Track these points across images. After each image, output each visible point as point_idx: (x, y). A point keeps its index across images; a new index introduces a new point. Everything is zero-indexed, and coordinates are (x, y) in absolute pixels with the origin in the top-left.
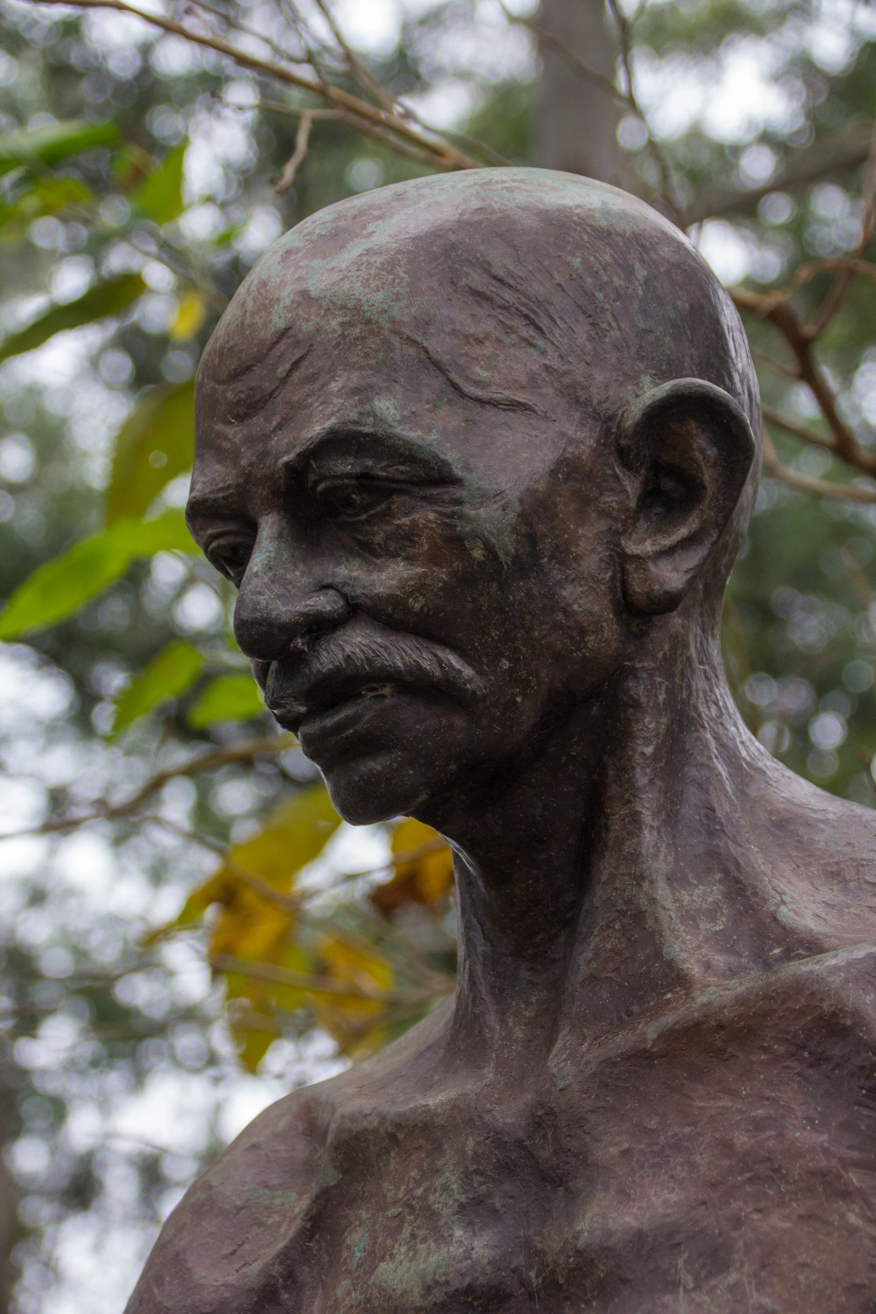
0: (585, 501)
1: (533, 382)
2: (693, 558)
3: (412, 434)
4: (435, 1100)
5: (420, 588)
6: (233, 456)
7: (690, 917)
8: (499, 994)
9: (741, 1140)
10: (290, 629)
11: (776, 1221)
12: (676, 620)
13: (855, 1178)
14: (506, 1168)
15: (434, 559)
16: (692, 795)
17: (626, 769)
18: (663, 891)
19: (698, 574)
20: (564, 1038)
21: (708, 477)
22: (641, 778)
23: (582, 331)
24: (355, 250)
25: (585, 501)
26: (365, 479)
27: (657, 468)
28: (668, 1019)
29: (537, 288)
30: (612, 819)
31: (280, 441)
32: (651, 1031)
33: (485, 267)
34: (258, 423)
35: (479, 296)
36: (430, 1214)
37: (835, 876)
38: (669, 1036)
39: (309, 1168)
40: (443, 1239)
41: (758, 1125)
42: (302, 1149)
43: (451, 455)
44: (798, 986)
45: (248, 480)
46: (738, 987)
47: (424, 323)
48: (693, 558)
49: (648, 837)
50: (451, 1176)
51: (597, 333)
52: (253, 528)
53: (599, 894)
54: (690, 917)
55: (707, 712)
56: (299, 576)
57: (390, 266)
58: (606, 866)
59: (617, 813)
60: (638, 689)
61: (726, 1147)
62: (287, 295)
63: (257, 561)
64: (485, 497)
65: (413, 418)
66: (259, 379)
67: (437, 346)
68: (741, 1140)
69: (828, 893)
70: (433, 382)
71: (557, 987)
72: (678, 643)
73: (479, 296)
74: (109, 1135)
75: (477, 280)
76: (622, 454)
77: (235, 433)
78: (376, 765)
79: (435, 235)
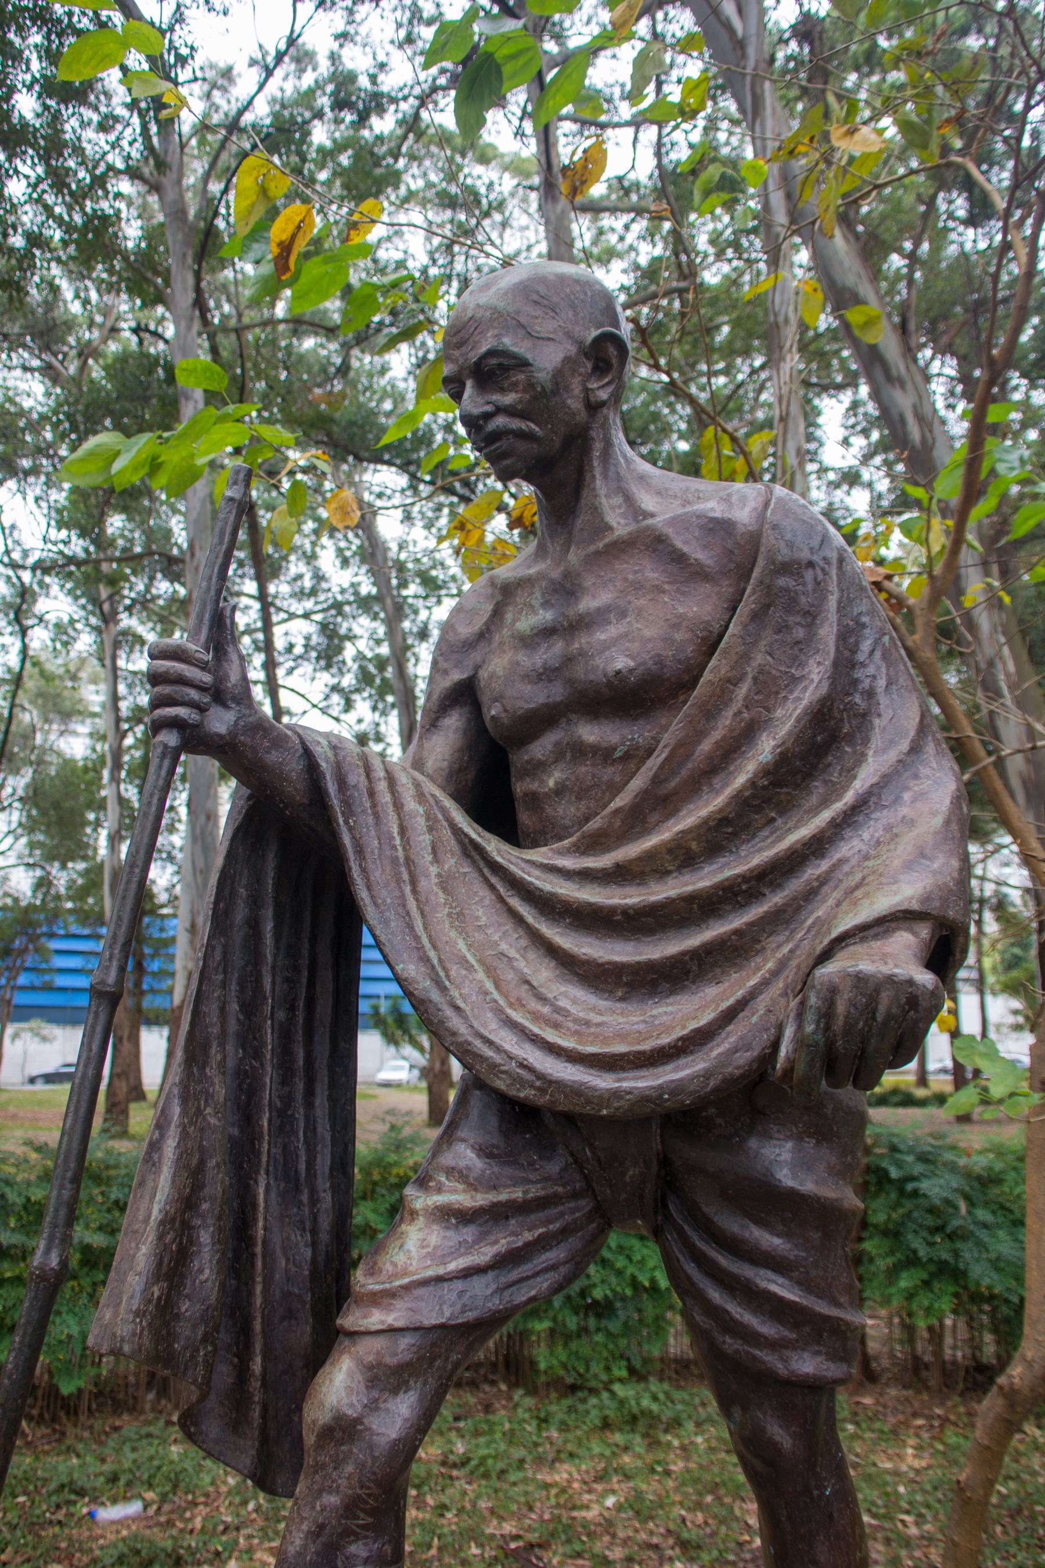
0: (574, 371)
1: (555, 332)
2: (610, 389)
3: (515, 349)
4: (532, 571)
5: (520, 401)
6: (456, 361)
7: (613, 508)
8: (551, 537)
9: (631, 577)
10: (478, 417)
11: (642, 601)
12: (605, 410)
13: (666, 587)
14: (555, 591)
15: (524, 391)
16: (612, 469)
17: (590, 460)
18: (603, 500)
19: (612, 395)
20: (573, 549)
21: (615, 361)
22: (596, 463)
23: (571, 314)
24: (494, 289)
25: (574, 371)
26: (500, 365)
27: (598, 359)
28: (606, 541)
29: (555, 299)
30: (535, 800)
31: (471, 354)
32: (601, 545)
33: (537, 293)
34: (464, 349)
35: (536, 303)
36: (532, 607)
37: (659, 493)
38: (607, 546)
39: (492, 596)
40: (535, 613)
41: (636, 572)
42: (490, 591)
43: (529, 356)
44: (648, 527)
45: (461, 369)
46: (629, 529)
47: (518, 312)
48: (610, 389)
49: (598, 483)
50: (538, 594)
51: (576, 314)
52: (463, 385)
53: (583, 502)
54: (613, 508)
55: (616, 441)
56: (480, 400)
57: (506, 294)
58: (585, 493)
59: (588, 476)
60: (593, 434)
61: (626, 579)
62: (472, 306)
63: (466, 395)
64: (540, 370)
65: (515, 344)
66: (464, 334)
67: (523, 319)
68: (631, 577)
69: (657, 499)
70: (522, 332)
71: (570, 533)
72: (606, 418)
73: (536, 303)
74: (871, 1260)
75: (535, 297)
76: (586, 355)
77: (456, 353)
78: (507, 462)
79: (521, 283)
